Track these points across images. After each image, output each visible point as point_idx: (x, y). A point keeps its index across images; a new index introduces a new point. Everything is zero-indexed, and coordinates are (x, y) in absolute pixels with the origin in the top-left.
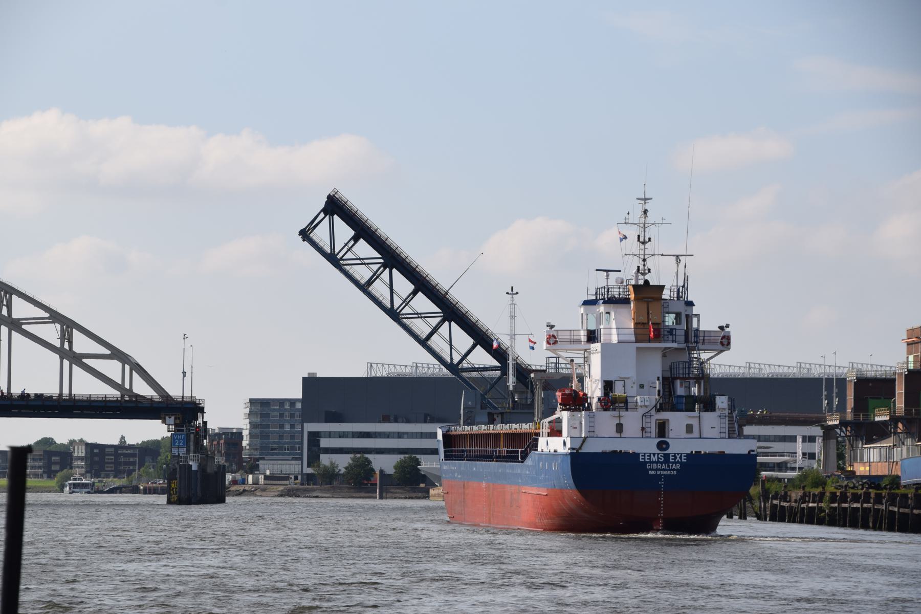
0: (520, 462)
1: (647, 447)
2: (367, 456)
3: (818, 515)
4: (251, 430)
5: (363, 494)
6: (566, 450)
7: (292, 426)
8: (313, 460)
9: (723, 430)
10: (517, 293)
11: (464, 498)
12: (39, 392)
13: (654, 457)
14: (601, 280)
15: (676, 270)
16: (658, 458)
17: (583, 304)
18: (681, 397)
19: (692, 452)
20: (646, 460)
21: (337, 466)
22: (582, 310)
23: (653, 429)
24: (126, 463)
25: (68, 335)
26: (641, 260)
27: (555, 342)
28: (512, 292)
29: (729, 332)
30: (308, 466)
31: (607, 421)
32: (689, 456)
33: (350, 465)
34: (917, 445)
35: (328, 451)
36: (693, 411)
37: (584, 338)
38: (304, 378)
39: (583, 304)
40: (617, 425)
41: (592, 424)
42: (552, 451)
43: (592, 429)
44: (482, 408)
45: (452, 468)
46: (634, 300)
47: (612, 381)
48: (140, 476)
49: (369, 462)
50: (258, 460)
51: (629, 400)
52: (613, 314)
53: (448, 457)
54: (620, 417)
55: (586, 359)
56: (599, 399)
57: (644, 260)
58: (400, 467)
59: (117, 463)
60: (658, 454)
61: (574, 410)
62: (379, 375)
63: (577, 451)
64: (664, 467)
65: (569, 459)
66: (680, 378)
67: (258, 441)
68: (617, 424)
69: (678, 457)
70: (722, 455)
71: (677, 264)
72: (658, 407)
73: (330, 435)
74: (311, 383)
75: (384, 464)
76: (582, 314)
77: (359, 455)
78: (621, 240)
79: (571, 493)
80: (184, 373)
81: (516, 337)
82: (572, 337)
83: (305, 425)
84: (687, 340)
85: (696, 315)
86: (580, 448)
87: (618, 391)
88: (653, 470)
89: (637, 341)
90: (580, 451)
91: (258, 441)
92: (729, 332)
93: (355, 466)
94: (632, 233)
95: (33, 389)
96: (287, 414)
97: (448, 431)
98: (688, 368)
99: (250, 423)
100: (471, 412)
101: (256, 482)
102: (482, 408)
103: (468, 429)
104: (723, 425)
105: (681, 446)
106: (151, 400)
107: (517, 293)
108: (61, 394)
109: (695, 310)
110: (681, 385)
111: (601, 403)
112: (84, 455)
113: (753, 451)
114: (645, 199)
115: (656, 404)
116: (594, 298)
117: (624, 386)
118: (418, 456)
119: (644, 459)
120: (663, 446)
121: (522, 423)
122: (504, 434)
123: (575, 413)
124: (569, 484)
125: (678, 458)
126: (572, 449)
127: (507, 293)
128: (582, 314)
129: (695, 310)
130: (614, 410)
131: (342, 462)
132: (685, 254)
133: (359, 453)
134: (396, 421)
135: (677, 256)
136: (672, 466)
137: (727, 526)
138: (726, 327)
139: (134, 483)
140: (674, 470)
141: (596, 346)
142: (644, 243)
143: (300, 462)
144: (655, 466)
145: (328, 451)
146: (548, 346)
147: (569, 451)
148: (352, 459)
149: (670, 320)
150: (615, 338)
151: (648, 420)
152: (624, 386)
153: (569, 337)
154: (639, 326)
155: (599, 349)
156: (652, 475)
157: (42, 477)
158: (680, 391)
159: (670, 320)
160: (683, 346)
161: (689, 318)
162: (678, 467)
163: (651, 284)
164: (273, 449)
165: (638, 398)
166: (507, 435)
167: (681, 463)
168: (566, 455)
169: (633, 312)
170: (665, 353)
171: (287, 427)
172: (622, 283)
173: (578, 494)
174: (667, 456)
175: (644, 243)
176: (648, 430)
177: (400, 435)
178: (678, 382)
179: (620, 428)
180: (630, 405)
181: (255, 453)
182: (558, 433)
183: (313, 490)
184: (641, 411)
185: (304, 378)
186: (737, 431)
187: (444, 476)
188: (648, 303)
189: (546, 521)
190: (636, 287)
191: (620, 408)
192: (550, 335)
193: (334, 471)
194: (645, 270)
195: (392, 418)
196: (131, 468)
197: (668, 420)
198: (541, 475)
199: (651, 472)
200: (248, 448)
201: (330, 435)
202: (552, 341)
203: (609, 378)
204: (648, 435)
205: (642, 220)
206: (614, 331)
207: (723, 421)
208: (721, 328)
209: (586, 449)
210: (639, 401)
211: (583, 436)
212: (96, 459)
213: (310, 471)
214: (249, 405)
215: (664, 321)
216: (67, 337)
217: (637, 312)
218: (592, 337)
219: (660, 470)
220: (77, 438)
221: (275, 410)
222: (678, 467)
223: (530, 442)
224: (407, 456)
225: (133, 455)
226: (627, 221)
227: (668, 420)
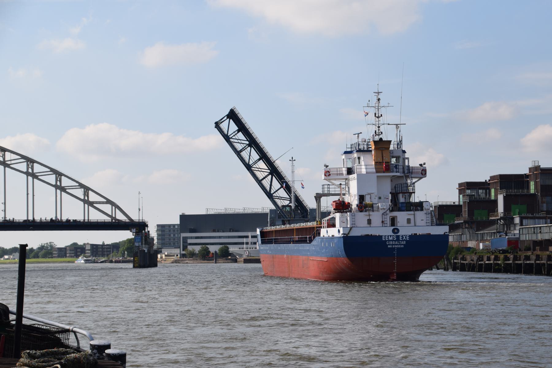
0: (308, 243)
1: (386, 232)
2: (207, 246)
3: (494, 267)
4: (157, 237)
5: (206, 261)
6: (340, 235)
7: (174, 235)
8: (185, 248)
9: (428, 221)
10: (295, 160)
11: (273, 264)
12: (75, 219)
13: (391, 237)
14: (355, 140)
15: (396, 133)
16: (393, 238)
17: (344, 153)
18: (402, 203)
19: (412, 234)
20: (386, 239)
21: (195, 250)
22: (344, 157)
23: (388, 222)
24: (107, 251)
25: (59, 179)
26: (377, 127)
27: (329, 175)
28: (292, 160)
29: (426, 167)
30: (183, 250)
31: (362, 218)
32: (411, 236)
33: (200, 250)
34: (476, 233)
35: (191, 244)
36: (333, 227)
37: (345, 172)
38: (180, 215)
39: (344, 153)
40: (368, 220)
41: (353, 220)
42: (331, 236)
43: (354, 223)
44: (279, 218)
45: (266, 248)
46: (374, 149)
47: (363, 195)
48: (113, 256)
49: (208, 248)
50: (161, 249)
51: (374, 205)
52: (362, 158)
53: (263, 242)
54: (369, 215)
55: (347, 184)
56: (357, 205)
57: (379, 127)
58: (221, 250)
59: (103, 251)
60: (393, 236)
61: (343, 212)
62: (211, 213)
63: (347, 235)
64: (396, 243)
65: (342, 240)
66: (402, 193)
67: (160, 241)
68: (368, 220)
69: (404, 237)
70: (429, 235)
71: (397, 129)
72: (391, 209)
73: (191, 238)
74: (183, 217)
75: (213, 249)
76: (343, 159)
77: (204, 246)
78: (366, 116)
79: (344, 259)
80: (139, 209)
81: (295, 182)
82: (338, 172)
83: (181, 234)
84: (404, 172)
85: (407, 158)
86: (349, 233)
87: (367, 201)
88: (390, 245)
89: (377, 172)
90: (348, 235)
91: (160, 241)
92: (426, 167)
93: (202, 250)
94: (372, 112)
95: (72, 218)
96: (172, 230)
97: (262, 230)
98: (406, 187)
99: (157, 234)
100: (274, 220)
101: (162, 258)
102: (279, 218)
103: (273, 228)
104: (428, 219)
105: (406, 231)
106: (125, 222)
107: (295, 160)
108: (84, 220)
109: (407, 155)
110: (403, 197)
111: (358, 208)
112: (90, 248)
113: (447, 233)
114: (378, 93)
115: (390, 208)
116: (349, 150)
117: (371, 198)
118: (228, 246)
119: (385, 239)
120: (395, 231)
121: (300, 223)
122: (296, 229)
123: (343, 214)
124: (342, 254)
125: (404, 238)
126: (343, 234)
127: (290, 160)
128: (343, 159)
129: (407, 155)
130: (366, 211)
131: (197, 249)
132: (400, 123)
133: (204, 245)
134: (218, 231)
135: (397, 125)
136: (401, 242)
137: (424, 277)
138: (424, 164)
139: (110, 259)
140: (402, 245)
141: (354, 176)
142: (378, 117)
143: (179, 249)
144: (391, 243)
145: (191, 244)
146: (325, 177)
147: (342, 235)
148: (201, 248)
149: (394, 161)
150: (364, 171)
151: (386, 217)
152: (371, 198)
153: (336, 172)
154: (377, 164)
155: (356, 177)
156: (390, 248)
157: (74, 257)
158: (402, 199)
159: (394, 161)
160: (402, 175)
161: (404, 159)
162: (405, 243)
163: (383, 140)
164: (166, 244)
165: (379, 204)
166: (297, 229)
167: (406, 241)
168: (340, 237)
169: (374, 156)
170: (393, 178)
171: (172, 235)
172: (365, 141)
173: (348, 260)
174: (398, 237)
175: (378, 117)
176: (386, 222)
177: (220, 237)
178: (401, 195)
179: (369, 222)
180: (375, 209)
181: (159, 246)
182: (334, 226)
183: (185, 260)
184: (382, 212)
185: (180, 215)
186: (435, 222)
187: (261, 252)
188: (382, 151)
189: (325, 276)
190: (375, 142)
191: (369, 210)
192: (326, 171)
193: (194, 252)
194: (379, 133)
195: (217, 230)
196: (108, 253)
197: (397, 216)
198: (323, 250)
199: (389, 246)
200: (156, 244)
201: (191, 238)
202: (327, 174)
203: (362, 193)
204: (386, 225)
205: (377, 105)
206: (363, 167)
207: (428, 216)
208: (421, 165)
209: (352, 234)
210: (380, 206)
211: (349, 226)
212: (95, 250)
213: (184, 252)
214: (156, 227)
215: (391, 161)
216: (58, 180)
217: (376, 156)
218: (350, 171)
219: (394, 245)
220: (86, 242)
221: (167, 229)
222: (405, 243)
223: (316, 232)
224: (223, 245)
225: (110, 248)
226: (368, 105)
227: (397, 216)
